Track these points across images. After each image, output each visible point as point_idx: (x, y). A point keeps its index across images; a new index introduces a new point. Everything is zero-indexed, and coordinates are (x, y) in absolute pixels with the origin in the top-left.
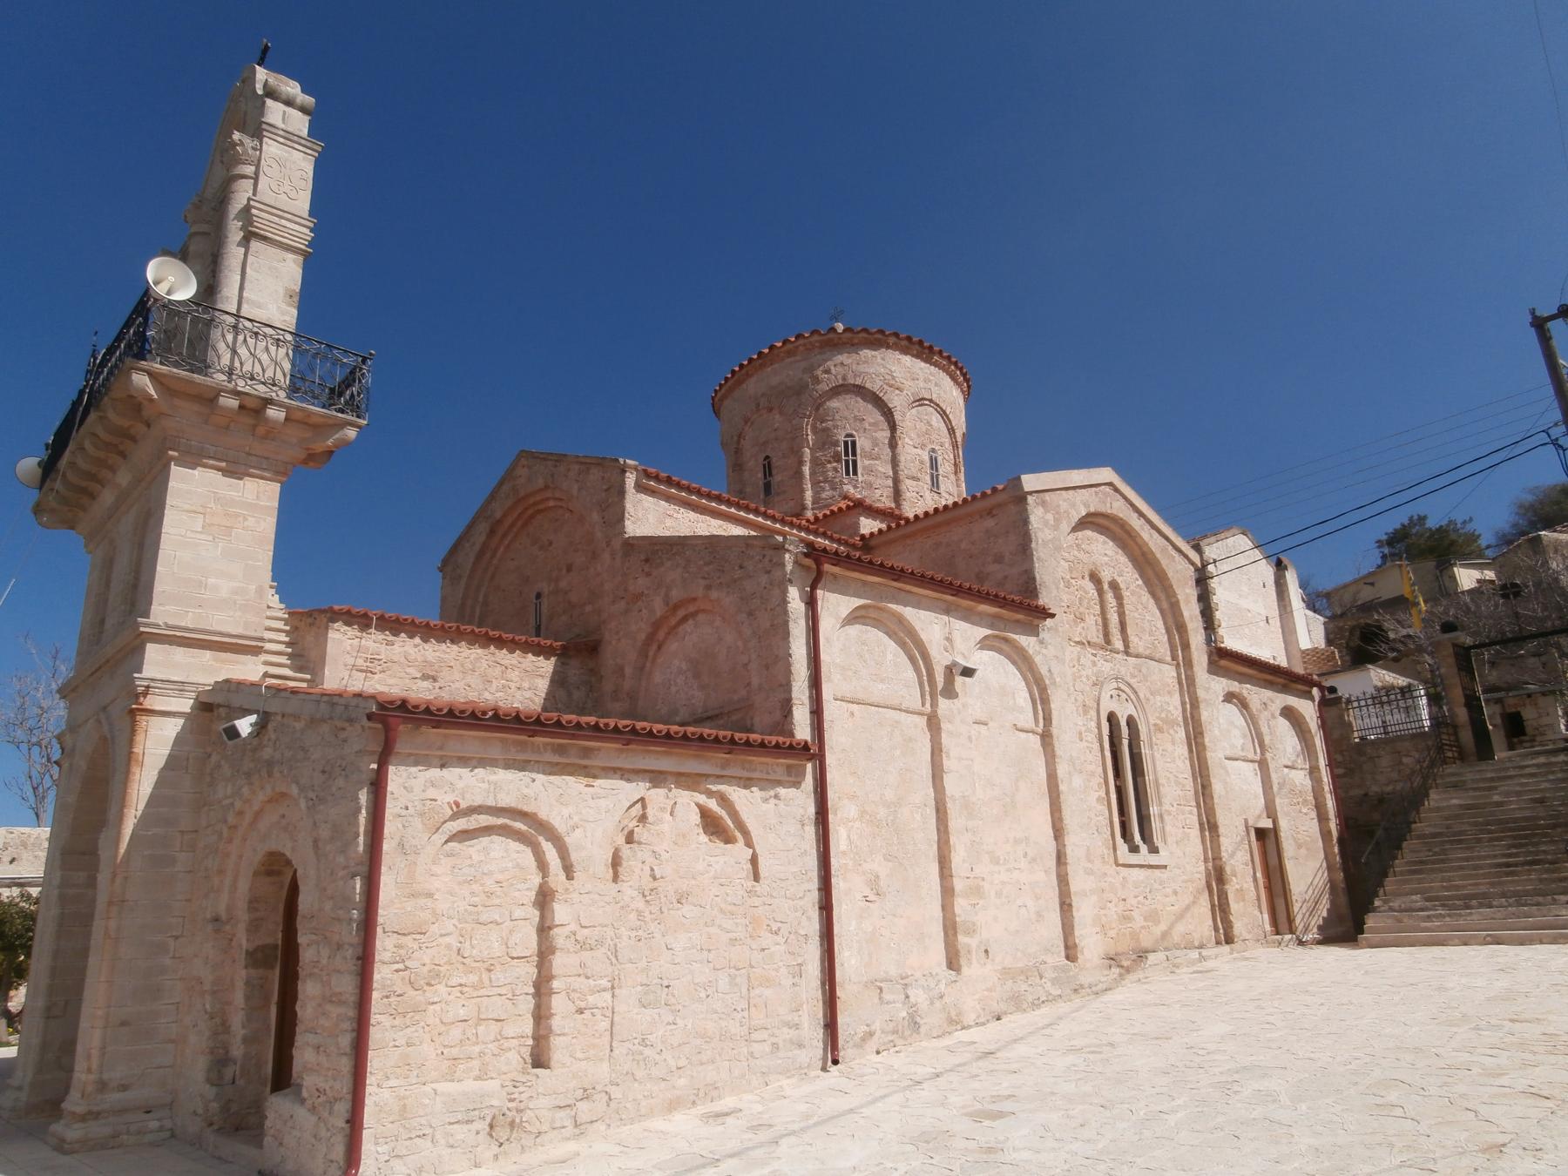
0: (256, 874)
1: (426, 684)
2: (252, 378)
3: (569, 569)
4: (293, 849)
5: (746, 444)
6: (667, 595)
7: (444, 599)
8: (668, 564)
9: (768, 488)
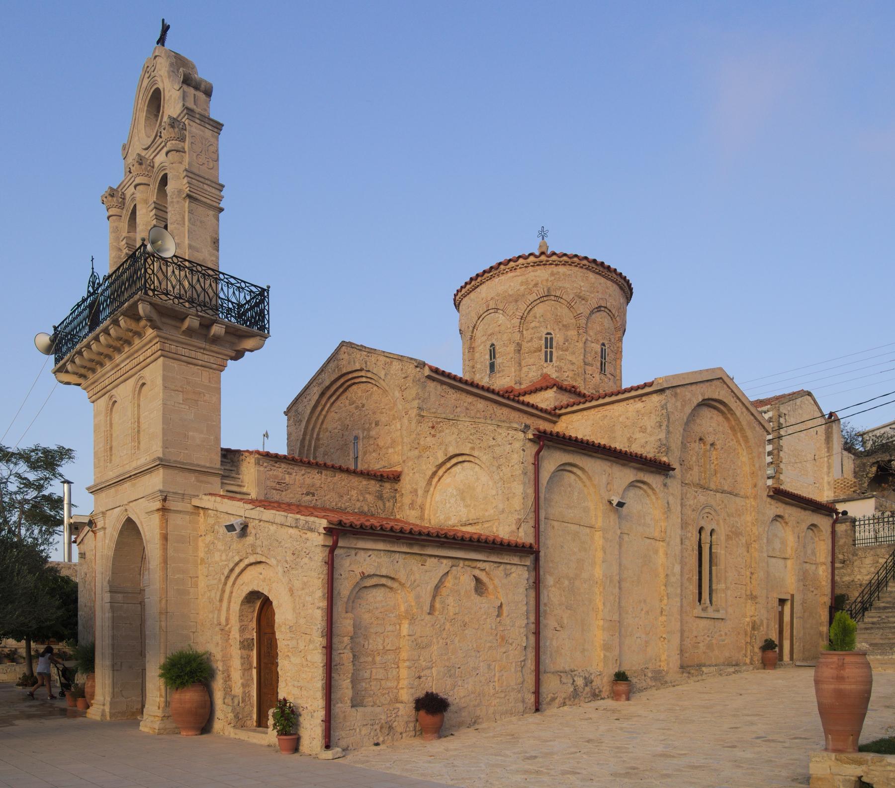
0: (243, 603)
1: (309, 498)
2: (205, 306)
3: (377, 424)
4: (269, 591)
5: (478, 333)
6: (446, 449)
7: (289, 435)
8: (447, 431)
9: (492, 366)
